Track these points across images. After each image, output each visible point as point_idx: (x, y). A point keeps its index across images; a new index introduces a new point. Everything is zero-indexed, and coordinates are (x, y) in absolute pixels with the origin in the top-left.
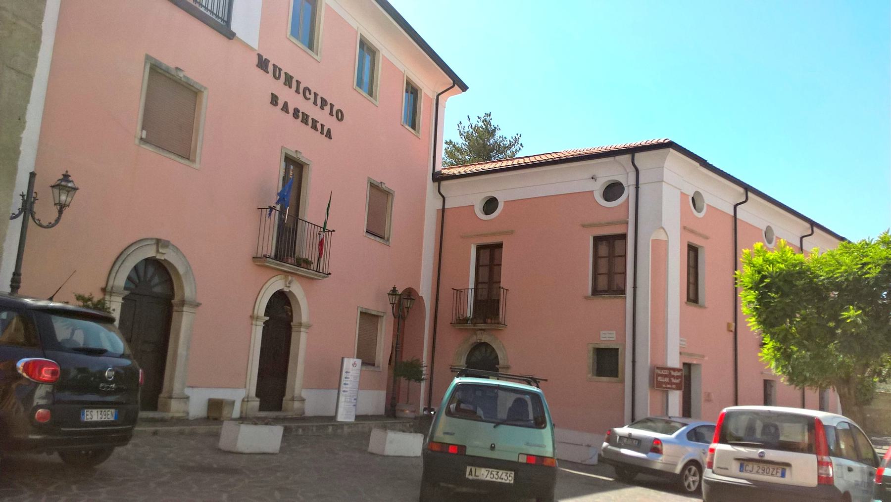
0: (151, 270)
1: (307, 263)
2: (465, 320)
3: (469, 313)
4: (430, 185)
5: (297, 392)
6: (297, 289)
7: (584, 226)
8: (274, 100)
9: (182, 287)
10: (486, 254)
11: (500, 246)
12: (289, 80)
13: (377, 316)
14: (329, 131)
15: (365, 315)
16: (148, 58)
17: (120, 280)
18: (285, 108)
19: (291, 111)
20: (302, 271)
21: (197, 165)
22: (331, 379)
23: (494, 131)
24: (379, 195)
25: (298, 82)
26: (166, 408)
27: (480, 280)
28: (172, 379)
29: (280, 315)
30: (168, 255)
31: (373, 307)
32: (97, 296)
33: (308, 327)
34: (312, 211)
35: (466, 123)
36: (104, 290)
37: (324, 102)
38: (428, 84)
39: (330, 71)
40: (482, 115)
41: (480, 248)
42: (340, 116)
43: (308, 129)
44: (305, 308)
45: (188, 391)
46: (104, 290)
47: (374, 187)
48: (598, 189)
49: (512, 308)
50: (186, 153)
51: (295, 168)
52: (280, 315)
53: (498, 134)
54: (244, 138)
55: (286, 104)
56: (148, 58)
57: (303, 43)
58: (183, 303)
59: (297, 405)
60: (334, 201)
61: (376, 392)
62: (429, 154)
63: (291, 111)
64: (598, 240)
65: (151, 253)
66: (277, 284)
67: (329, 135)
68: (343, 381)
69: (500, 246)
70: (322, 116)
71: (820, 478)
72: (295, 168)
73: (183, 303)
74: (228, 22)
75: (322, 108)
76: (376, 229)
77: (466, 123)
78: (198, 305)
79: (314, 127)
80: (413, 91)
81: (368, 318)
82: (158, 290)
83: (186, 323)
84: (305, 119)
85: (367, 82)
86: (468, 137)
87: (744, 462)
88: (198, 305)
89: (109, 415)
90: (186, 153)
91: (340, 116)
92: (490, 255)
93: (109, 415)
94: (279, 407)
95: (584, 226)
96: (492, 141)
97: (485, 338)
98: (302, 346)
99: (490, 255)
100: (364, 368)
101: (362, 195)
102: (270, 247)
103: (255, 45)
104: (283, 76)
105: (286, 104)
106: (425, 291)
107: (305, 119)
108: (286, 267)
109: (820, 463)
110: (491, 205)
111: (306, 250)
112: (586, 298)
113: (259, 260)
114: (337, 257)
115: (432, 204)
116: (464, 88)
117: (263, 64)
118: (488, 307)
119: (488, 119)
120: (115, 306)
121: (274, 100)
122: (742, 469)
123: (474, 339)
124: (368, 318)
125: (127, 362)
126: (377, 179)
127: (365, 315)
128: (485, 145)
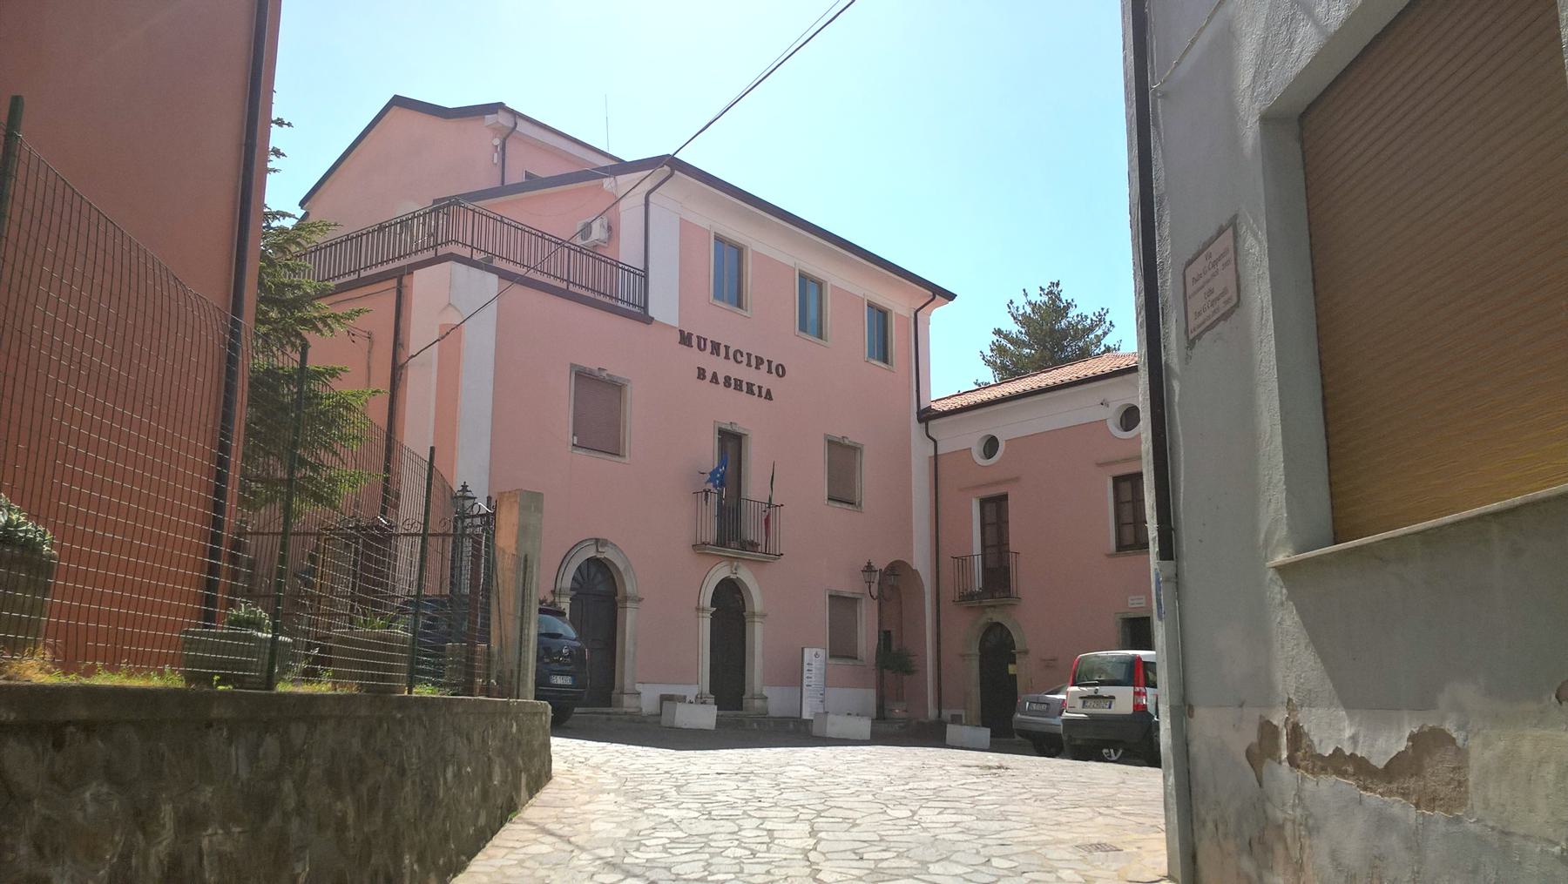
0: (593, 570)
1: (753, 546)
2: (971, 596)
3: (978, 584)
4: (916, 428)
5: (757, 690)
6: (745, 575)
7: (1100, 465)
8: (701, 374)
9: (623, 583)
10: (990, 508)
11: (1004, 497)
12: (716, 347)
13: (855, 600)
14: (768, 392)
15: (836, 599)
16: (572, 366)
17: (567, 582)
18: (715, 379)
19: (721, 380)
20: (747, 555)
21: (627, 460)
22: (794, 678)
23: (1069, 305)
24: (843, 456)
25: (727, 348)
26: (620, 703)
27: (989, 543)
28: (622, 673)
29: (730, 608)
30: (608, 554)
31: (846, 587)
32: (550, 599)
33: (764, 616)
34: (755, 487)
35: (1020, 301)
36: (553, 592)
37: (760, 361)
38: (898, 303)
39: (766, 323)
40: (1046, 286)
41: (984, 502)
42: (781, 371)
43: (743, 395)
44: (757, 599)
45: (639, 687)
46: (553, 592)
47: (834, 445)
48: (1111, 415)
49: (1024, 575)
50: (615, 451)
51: (731, 442)
52: (730, 608)
53: (1072, 313)
54: (672, 424)
55: (715, 376)
56: (572, 366)
57: (731, 303)
58: (626, 599)
59: (758, 703)
60: (785, 473)
61: (848, 691)
62: (910, 387)
63: (721, 380)
64: (1117, 480)
65: (592, 553)
66: (721, 572)
67: (769, 396)
68: (806, 674)
69: (1004, 497)
70: (760, 378)
71: (1137, 706)
72: (731, 442)
73: (626, 599)
74: (645, 308)
75: (757, 368)
76: (842, 492)
77: (1020, 301)
78: (641, 600)
79: (750, 391)
80: (880, 317)
81: (841, 604)
82: (601, 588)
83: (631, 619)
84: (738, 385)
85: (811, 320)
86: (1025, 321)
87: (1085, 698)
88: (641, 600)
89: (567, 680)
90: (615, 451)
91: (781, 371)
92: (995, 509)
93: (567, 680)
94: (740, 707)
95: (1100, 465)
96: (1064, 323)
97: (997, 617)
98: (758, 635)
99: (995, 509)
100: (833, 661)
101: (819, 457)
102: (710, 533)
103: (675, 323)
104: (709, 345)
105: (715, 376)
106: (921, 561)
107: (738, 385)
108: (729, 552)
109: (1137, 694)
110: (991, 445)
111: (752, 531)
112: (1110, 556)
113: (699, 547)
114: (788, 532)
115: (920, 452)
116: (950, 296)
117: (685, 339)
118: (998, 577)
119: (1055, 290)
120: (565, 604)
121: (701, 374)
122: (1084, 706)
123: (984, 620)
124: (841, 604)
125: (577, 644)
126: (837, 434)
127: (836, 599)
128: (1052, 331)
